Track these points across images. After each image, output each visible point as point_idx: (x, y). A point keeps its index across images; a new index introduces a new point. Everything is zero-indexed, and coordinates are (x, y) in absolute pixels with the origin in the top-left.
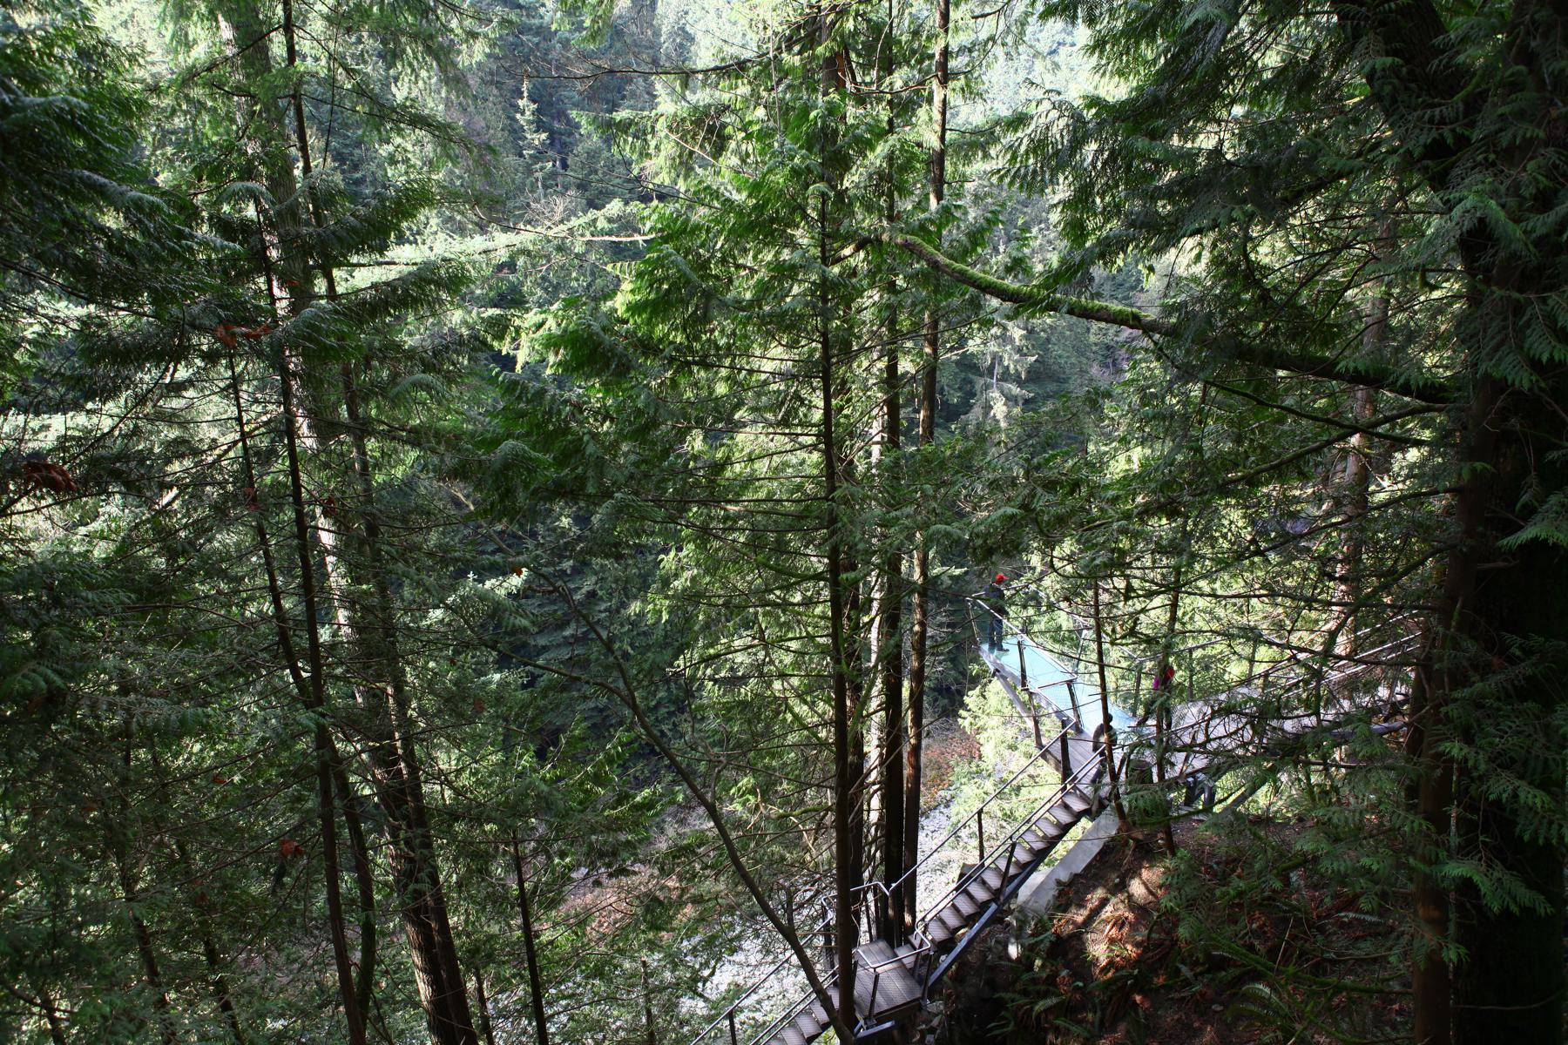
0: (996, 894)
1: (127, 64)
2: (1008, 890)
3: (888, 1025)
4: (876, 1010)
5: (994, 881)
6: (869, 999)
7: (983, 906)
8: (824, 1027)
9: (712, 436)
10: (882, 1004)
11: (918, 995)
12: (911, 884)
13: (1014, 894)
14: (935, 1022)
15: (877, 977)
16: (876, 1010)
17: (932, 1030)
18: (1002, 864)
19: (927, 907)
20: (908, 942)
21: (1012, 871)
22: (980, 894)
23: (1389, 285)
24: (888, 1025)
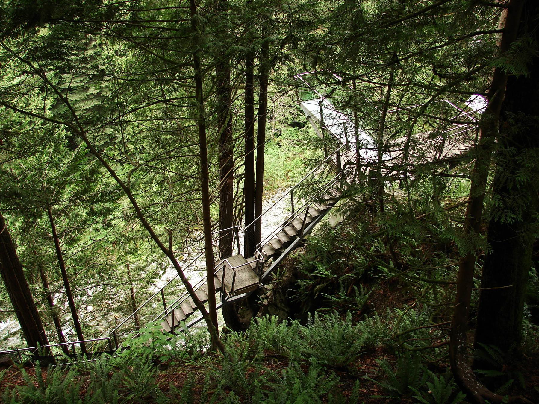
0: (299, 233)
1: (469, 48)
2: (305, 231)
3: (243, 295)
4: (235, 289)
5: (298, 227)
6: (231, 283)
7: (292, 239)
8: (195, 310)
9: (25, 25)
10: (238, 285)
11: (257, 281)
12: (259, 223)
13: (309, 232)
14: (269, 293)
15: (235, 273)
16: (235, 289)
17: (267, 298)
18: (303, 217)
19: (268, 233)
20: (253, 255)
21: (308, 221)
22: (291, 233)
23: (59, 307)
24: (243, 295)
